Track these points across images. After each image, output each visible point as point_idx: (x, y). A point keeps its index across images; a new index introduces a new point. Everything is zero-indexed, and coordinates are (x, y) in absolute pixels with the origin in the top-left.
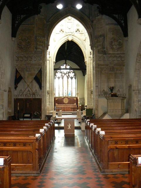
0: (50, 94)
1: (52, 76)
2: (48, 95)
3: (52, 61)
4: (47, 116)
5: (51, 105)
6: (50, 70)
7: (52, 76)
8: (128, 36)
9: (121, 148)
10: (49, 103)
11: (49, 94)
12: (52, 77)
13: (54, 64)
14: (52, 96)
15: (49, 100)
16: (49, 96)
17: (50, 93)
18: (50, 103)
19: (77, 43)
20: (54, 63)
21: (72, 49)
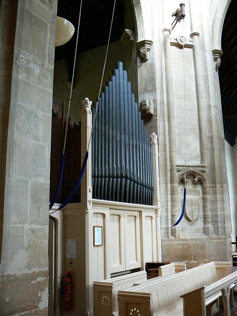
0: (208, 184)
1: (209, 107)
2: (199, 188)
3: (207, 48)
4: (183, 15)
5: (216, 231)
6: (201, 82)
7: (209, 107)
8: (57, 48)
9: (226, 199)
10: (205, 222)
11: (201, 182)
12: (213, 109)
13: (215, 60)
14: (215, 193)
15: (204, 211)
16: (204, 193)
17: (207, 177)
18: (210, 226)
19: (50, 153)
20: (217, 56)
21: (144, 144)
